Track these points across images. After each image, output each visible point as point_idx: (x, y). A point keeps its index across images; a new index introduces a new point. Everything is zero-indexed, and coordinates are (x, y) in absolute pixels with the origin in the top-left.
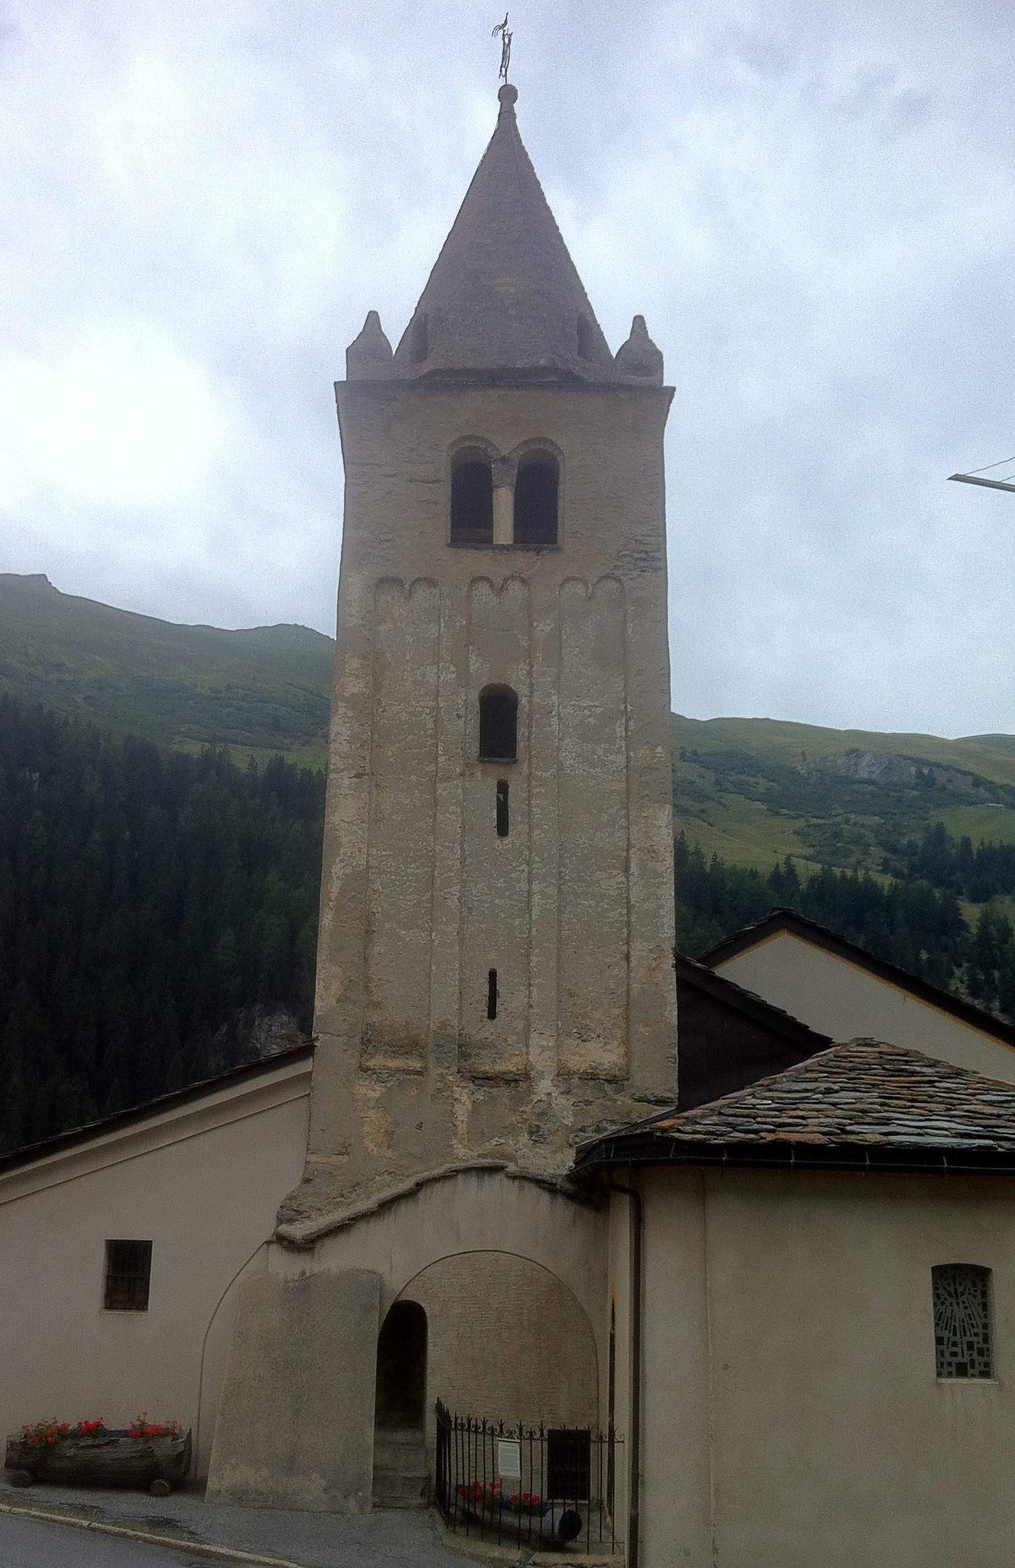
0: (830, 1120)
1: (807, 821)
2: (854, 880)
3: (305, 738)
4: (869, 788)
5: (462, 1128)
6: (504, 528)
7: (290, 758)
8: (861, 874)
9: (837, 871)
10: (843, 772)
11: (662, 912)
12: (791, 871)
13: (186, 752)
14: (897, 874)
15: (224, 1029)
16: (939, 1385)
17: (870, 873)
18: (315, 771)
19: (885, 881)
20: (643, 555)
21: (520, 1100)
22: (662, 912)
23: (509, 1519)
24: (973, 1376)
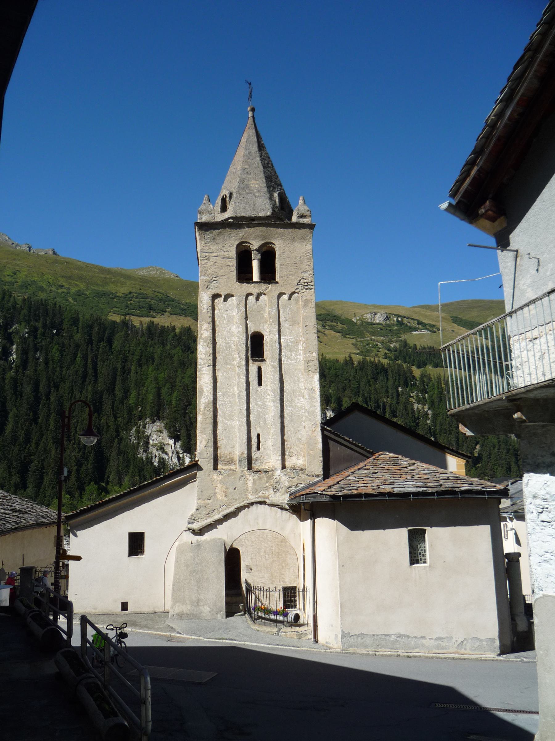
0: (375, 484)
1: (357, 339)
2: (374, 362)
3: (162, 312)
4: (380, 326)
5: (250, 489)
6: (256, 276)
7: (155, 320)
8: (377, 359)
9: (368, 358)
10: (369, 320)
11: (316, 411)
12: (351, 359)
13: (114, 320)
14: (390, 359)
15: (134, 429)
16: (411, 567)
17: (380, 359)
18: (166, 326)
19: (385, 362)
20: (306, 284)
21: (270, 478)
22: (316, 411)
23: (272, 617)
24: (421, 563)
